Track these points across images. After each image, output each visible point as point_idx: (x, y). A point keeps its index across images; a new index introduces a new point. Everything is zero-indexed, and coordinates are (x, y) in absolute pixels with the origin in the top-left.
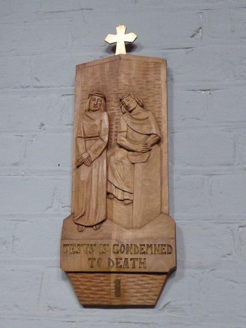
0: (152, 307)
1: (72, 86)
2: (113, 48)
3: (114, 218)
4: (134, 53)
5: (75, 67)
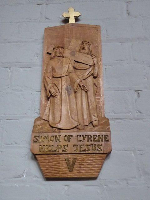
0: (95, 178)
1: (41, 39)
2: (66, 20)
3: (70, 96)
4: (78, 23)
5: (43, 31)
